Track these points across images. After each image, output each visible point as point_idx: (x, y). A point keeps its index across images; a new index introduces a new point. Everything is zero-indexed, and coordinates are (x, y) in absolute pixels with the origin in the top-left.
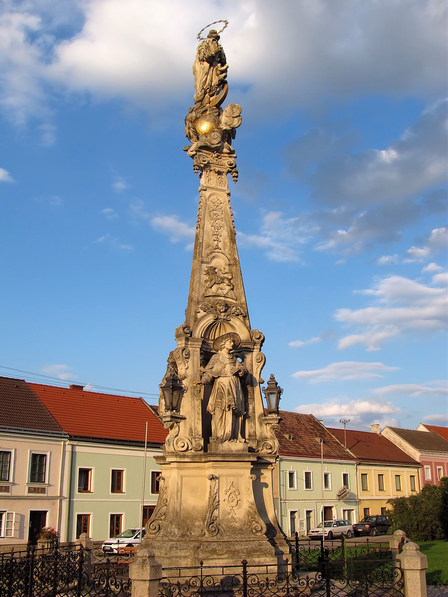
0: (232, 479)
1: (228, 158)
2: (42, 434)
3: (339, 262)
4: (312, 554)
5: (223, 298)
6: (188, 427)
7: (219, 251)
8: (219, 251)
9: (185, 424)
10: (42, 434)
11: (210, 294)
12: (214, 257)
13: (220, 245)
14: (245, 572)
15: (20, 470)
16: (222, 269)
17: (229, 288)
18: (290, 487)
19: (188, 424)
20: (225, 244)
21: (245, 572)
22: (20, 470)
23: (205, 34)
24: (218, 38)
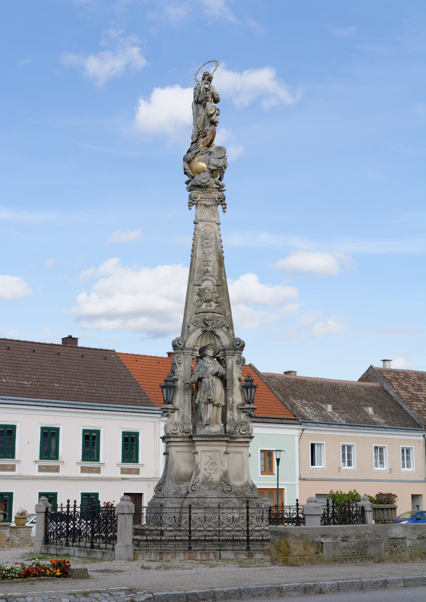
0: (210, 454)
1: (218, 192)
2: (204, 439)
3: (403, 523)
4: (236, 523)
5: (211, 314)
6: (181, 415)
7: (209, 274)
8: (209, 274)
9: (179, 413)
10: (204, 439)
11: (201, 311)
12: (204, 280)
13: (210, 269)
14: (248, 512)
15: (28, 444)
16: (211, 289)
17: (216, 305)
18: (312, 465)
19: (181, 413)
20: (213, 268)
21: (248, 512)
22: (28, 444)
23: (200, 76)
24: (210, 80)
